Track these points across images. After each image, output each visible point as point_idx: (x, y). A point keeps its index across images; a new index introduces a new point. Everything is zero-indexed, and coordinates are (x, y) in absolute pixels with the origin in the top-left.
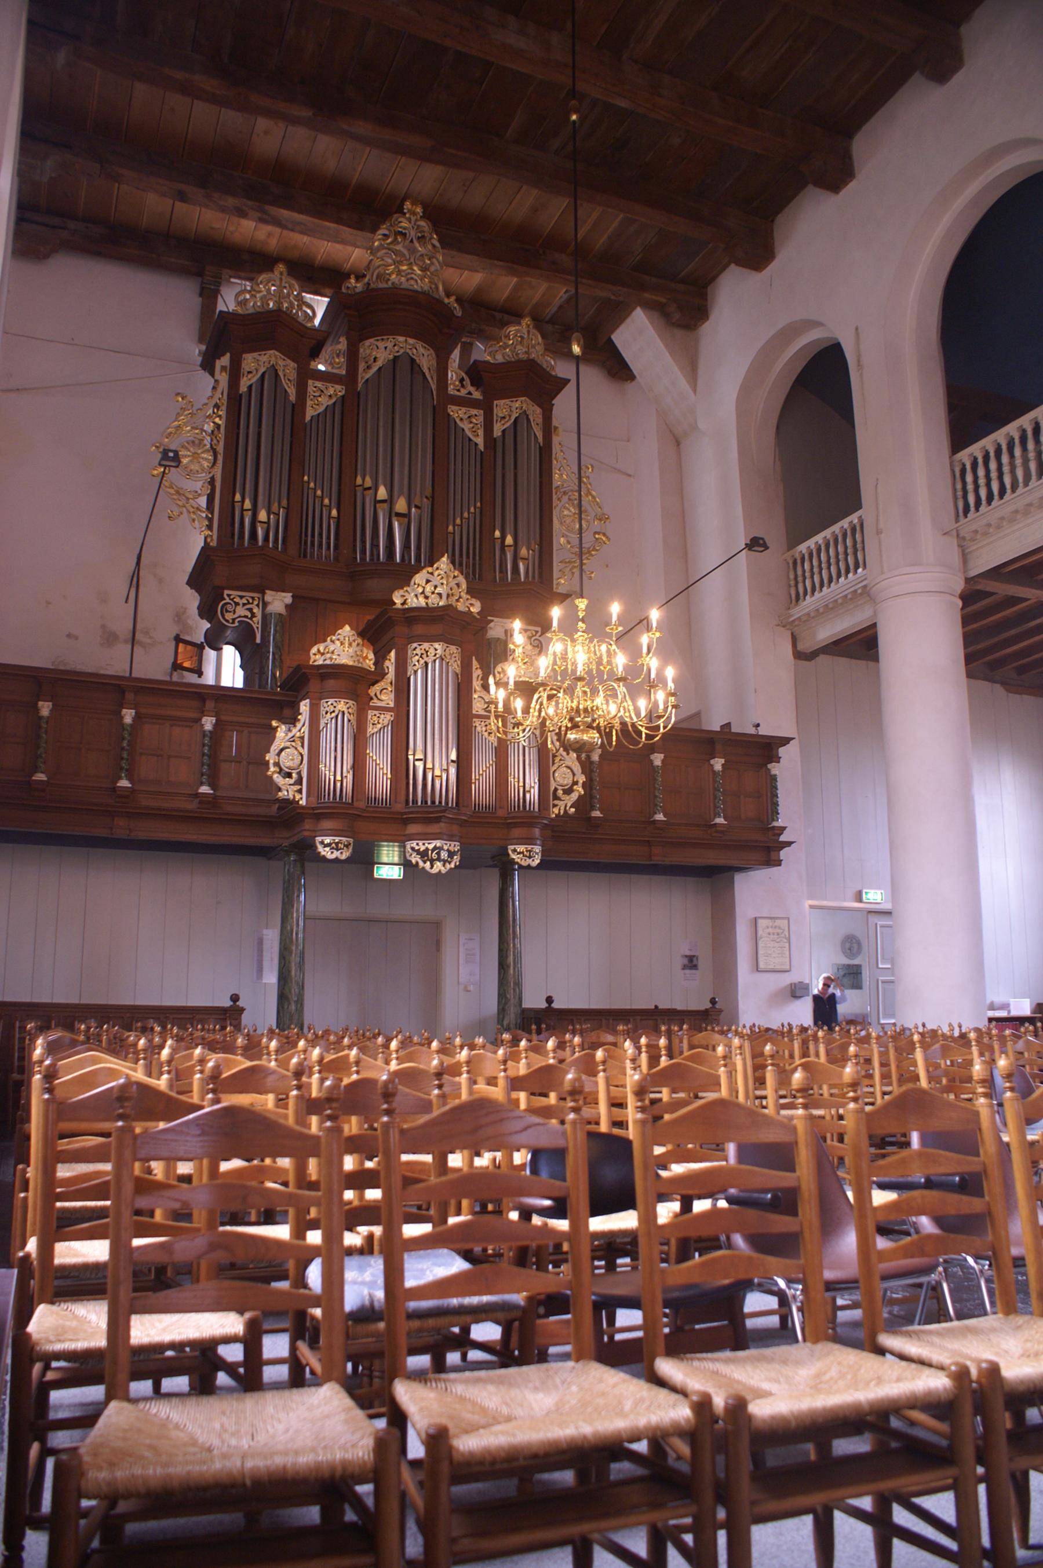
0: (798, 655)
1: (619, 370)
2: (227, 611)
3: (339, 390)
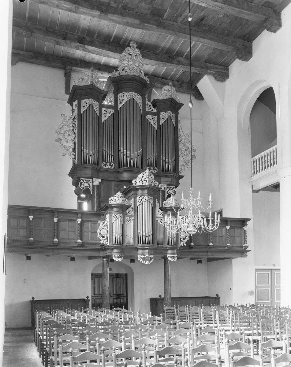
0: (254, 191)
1: (199, 96)
2: (82, 185)
3: (112, 111)
